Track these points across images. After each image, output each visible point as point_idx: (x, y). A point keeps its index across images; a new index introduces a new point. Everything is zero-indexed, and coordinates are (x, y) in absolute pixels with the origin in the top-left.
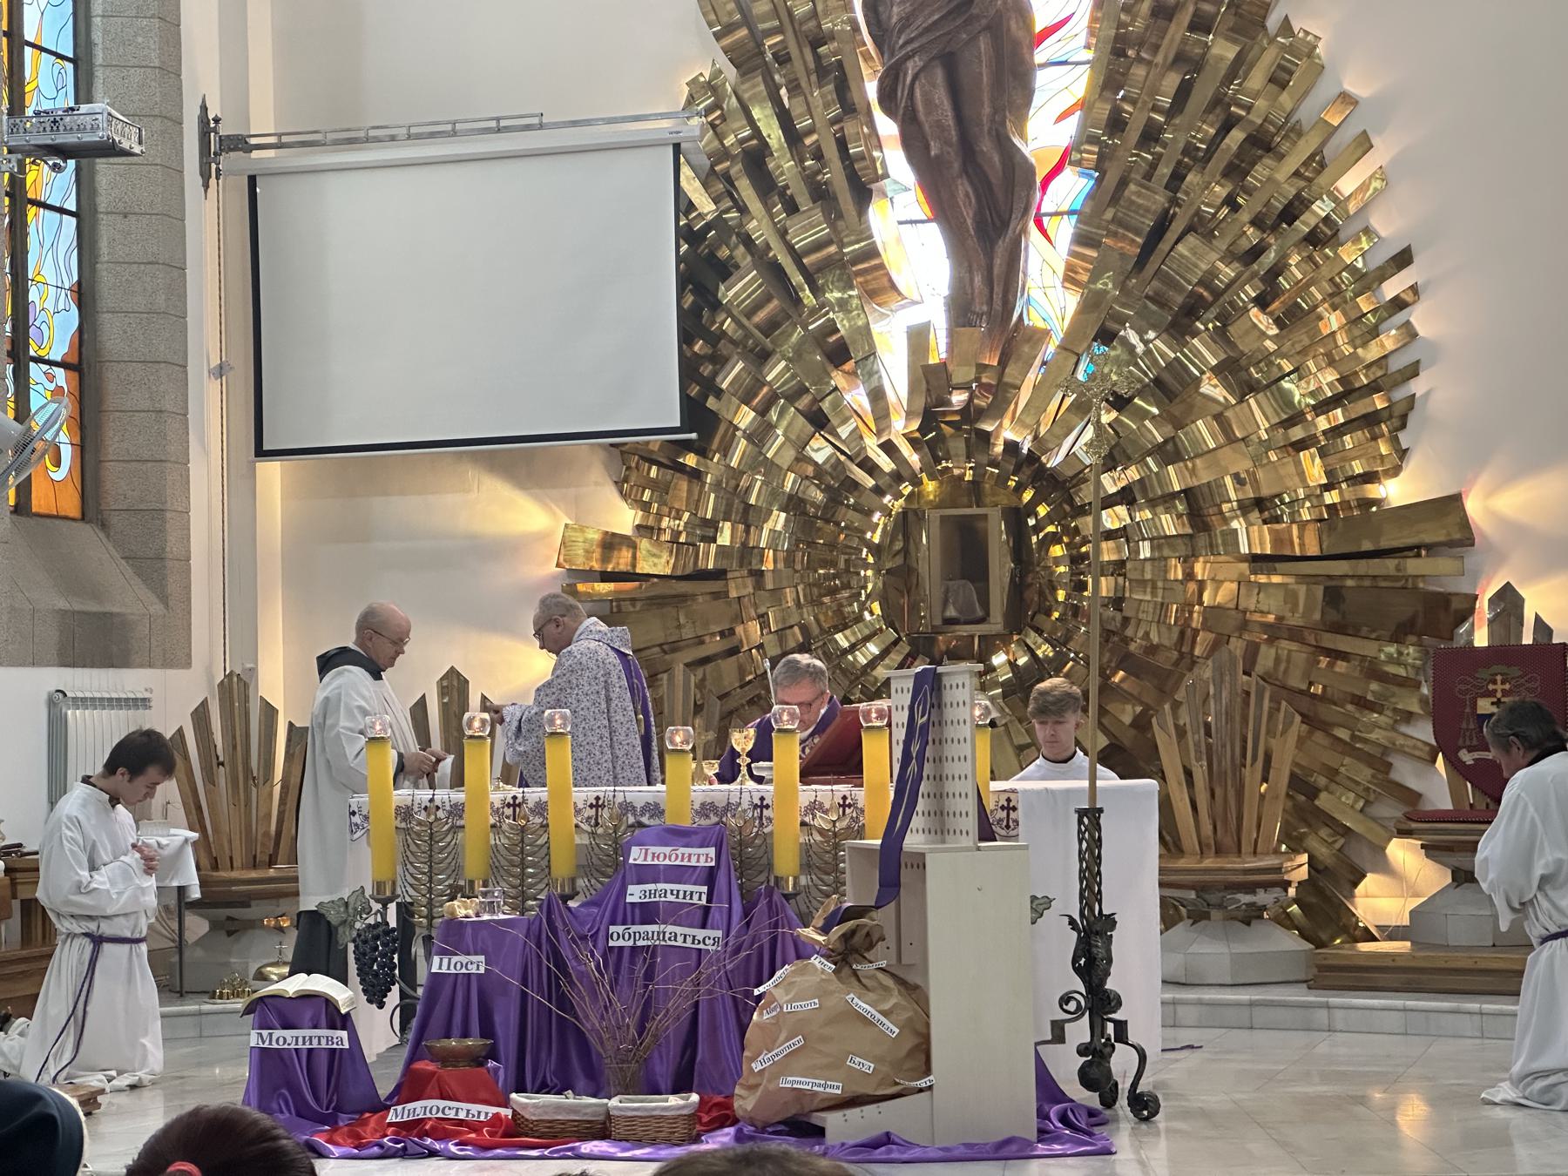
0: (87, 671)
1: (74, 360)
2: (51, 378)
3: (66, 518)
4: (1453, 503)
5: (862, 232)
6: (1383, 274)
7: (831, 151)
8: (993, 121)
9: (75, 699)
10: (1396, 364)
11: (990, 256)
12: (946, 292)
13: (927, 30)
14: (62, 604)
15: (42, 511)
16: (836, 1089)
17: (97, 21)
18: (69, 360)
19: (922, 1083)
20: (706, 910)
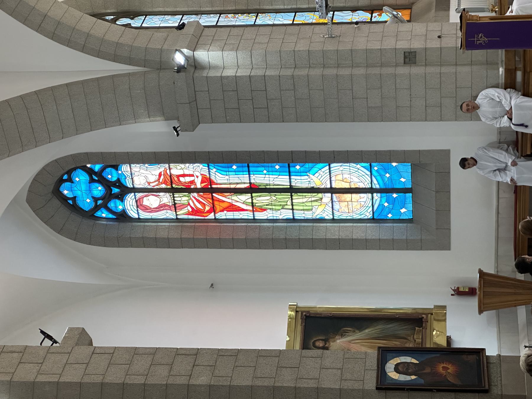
0: (451, 5)
1: (370, 12)
2: (375, 17)
3: (411, 12)
9: (458, 6)
14: (433, 11)
15: (409, 18)
17: (285, 7)
18: (371, 13)
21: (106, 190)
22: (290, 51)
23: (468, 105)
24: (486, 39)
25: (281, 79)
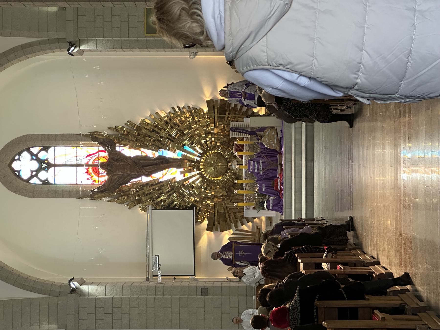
4: (208, 102)
5: (167, 182)
6: (175, 110)
7: (153, 187)
8: (152, 161)
10: (188, 109)
11: (171, 162)
12: (176, 169)
13: (139, 169)
16: (276, 136)
19: (275, 127)
20: (258, 162)
21: (40, 164)
22: (137, 286)
23: (236, 320)
24: (245, 254)
25: (130, 300)
